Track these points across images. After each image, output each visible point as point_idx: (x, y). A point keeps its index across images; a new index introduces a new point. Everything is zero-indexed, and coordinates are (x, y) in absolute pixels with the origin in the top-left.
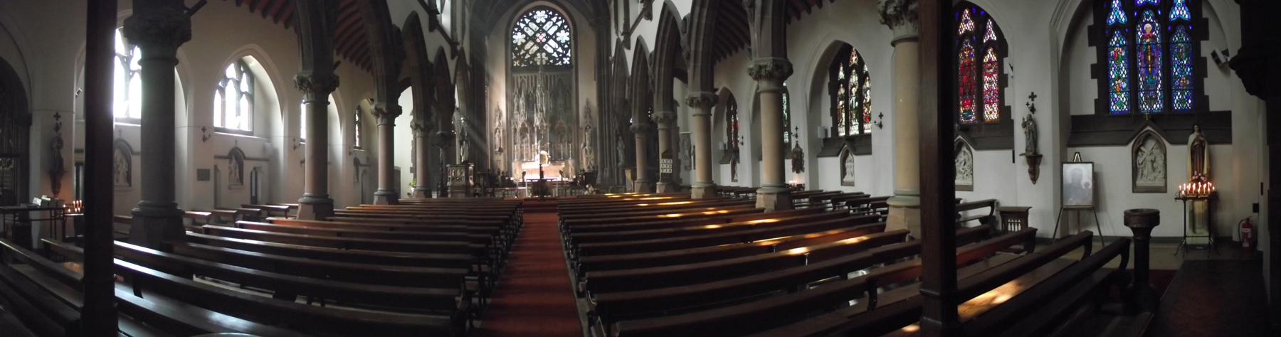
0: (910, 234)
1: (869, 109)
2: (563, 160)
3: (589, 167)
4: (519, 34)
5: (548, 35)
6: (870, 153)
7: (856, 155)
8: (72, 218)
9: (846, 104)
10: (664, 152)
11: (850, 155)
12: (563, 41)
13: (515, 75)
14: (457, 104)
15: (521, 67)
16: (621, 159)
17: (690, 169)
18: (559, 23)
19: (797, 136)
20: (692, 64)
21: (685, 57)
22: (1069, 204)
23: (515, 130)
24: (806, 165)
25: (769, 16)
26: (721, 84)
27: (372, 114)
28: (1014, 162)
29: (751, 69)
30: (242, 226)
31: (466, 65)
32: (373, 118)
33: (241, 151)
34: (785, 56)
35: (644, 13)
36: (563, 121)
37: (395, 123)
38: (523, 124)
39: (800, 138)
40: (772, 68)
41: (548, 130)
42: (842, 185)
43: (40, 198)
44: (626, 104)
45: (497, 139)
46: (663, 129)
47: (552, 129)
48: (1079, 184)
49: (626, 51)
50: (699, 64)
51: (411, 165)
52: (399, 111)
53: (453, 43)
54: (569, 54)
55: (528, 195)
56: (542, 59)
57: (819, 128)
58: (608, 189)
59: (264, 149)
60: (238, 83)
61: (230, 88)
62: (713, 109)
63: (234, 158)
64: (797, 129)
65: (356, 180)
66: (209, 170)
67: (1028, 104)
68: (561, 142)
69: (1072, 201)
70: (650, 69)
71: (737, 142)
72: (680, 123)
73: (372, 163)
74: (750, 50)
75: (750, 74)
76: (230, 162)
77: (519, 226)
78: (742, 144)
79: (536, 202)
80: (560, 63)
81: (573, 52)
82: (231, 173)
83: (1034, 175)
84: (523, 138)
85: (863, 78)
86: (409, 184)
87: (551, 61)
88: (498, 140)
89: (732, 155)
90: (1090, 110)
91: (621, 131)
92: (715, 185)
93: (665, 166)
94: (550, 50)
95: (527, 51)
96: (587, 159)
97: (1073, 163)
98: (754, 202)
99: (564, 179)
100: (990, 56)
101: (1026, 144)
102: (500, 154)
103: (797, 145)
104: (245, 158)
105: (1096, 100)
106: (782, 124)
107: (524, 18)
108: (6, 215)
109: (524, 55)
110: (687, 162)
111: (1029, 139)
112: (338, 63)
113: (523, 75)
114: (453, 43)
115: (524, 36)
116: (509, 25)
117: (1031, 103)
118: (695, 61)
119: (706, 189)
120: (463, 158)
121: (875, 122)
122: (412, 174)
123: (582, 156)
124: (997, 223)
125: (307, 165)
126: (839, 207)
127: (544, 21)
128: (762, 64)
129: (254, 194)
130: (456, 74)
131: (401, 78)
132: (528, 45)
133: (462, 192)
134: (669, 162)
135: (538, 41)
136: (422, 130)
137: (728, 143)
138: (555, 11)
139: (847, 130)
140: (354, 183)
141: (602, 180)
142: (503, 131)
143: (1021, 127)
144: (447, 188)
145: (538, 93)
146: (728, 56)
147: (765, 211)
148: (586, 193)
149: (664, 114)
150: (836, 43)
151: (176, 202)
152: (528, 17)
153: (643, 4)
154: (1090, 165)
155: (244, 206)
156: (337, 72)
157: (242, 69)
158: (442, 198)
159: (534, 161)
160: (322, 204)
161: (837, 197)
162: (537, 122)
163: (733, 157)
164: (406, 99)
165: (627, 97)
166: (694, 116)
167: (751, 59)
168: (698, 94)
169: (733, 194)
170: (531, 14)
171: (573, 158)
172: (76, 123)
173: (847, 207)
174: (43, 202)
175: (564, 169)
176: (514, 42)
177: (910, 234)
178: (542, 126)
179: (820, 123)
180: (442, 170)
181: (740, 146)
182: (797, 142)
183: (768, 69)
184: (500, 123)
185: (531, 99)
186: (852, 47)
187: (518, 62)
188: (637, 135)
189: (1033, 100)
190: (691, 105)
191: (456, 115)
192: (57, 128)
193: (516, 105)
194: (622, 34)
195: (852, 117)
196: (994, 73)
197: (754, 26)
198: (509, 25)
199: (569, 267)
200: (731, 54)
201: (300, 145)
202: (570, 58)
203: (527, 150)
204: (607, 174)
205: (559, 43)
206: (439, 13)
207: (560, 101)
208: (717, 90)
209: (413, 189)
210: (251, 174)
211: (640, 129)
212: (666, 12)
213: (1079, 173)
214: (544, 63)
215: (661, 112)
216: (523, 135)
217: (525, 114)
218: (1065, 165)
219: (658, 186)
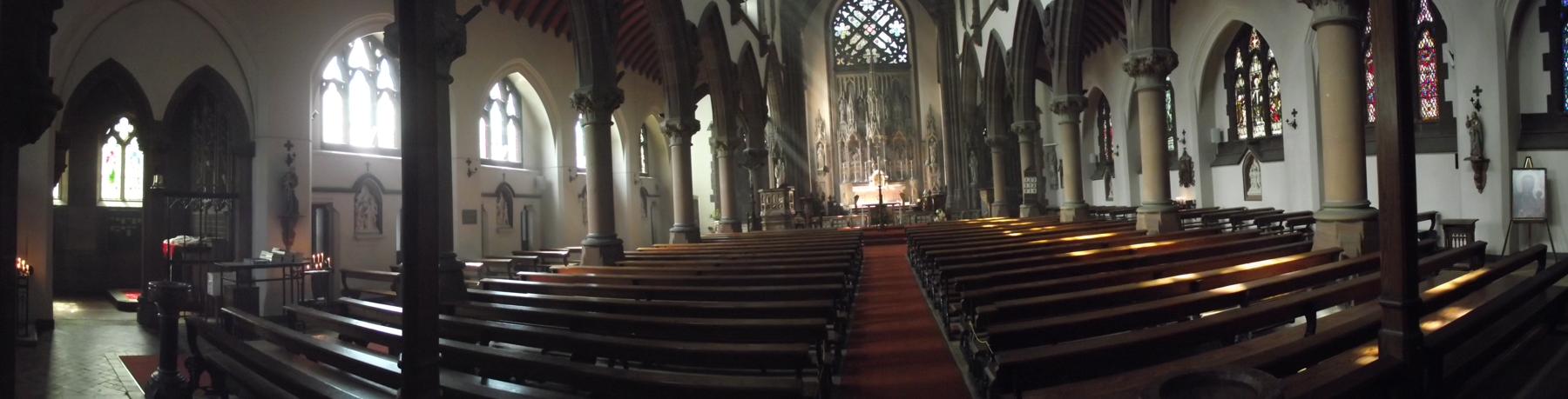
0: (1344, 253)
1: (1277, 105)
3: (934, 189)
4: (842, 24)
5: (878, 26)
6: (1282, 159)
7: (1263, 161)
8: (310, 276)
9: (1247, 99)
10: (1027, 170)
11: (1255, 162)
12: (897, 35)
13: (839, 76)
14: (769, 114)
15: (846, 65)
17: (1057, 188)
18: (892, 12)
19: (1184, 142)
20: (1056, 62)
22: (1519, 217)
23: (843, 143)
24: (1197, 177)
26: (1090, 83)
27: (663, 132)
28: (1457, 167)
29: (1126, 64)
30: (524, 278)
31: (778, 63)
32: (662, 137)
33: (511, 188)
34: (1169, 43)
37: (692, 142)
38: (852, 137)
39: (1188, 143)
41: (884, 144)
42: (1245, 199)
43: (270, 252)
45: (820, 155)
47: (888, 143)
48: (1531, 194)
49: (976, 47)
50: (1065, 62)
51: (711, 192)
52: (696, 127)
53: (761, 36)
54: (905, 50)
56: (872, 56)
57: (1212, 131)
58: (959, 214)
59: (535, 183)
60: (503, 105)
61: (495, 111)
62: (1082, 115)
63: (501, 195)
64: (1184, 133)
65: (644, 215)
66: (475, 211)
67: (1472, 100)
68: (900, 157)
69: (1523, 213)
70: (1007, 70)
71: (1110, 152)
72: (1043, 134)
73: (663, 193)
74: (1125, 41)
75: (1126, 71)
76: (498, 202)
77: (861, 263)
78: (1117, 154)
80: (895, 61)
81: (910, 47)
82: (498, 214)
83: (1480, 182)
85: (1268, 65)
86: (710, 217)
87: (884, 59)
88: (820, 157)
89: (1105, 168)
90: (1542, 108)
91: (973, 144)
92: (1088, 205)
94: (882, 46)
95: (854, 46)
96: (932, 178)
97: (1524, 169)
98: (1134, 223)
99: (907, 204)
100: (1426, 41)
101: (1472, 146)
102: (825, 174)
103: (1185, 153)
104: (515, 196)
105: (1548, 96)
106: (1165, 128)
107: (847, 6)
108: (224, 274)
109: (850, 51)
110: (1054, 179)
111: (1474, 141)
112: (622, 74)
113: (849, 76)
114: (761, 36)
115: (849, 27)
117: (1475, 98)
118: (1060, 59)
121: (1288, 121)
122: (713, 204)
123: (926, 174)
124: (1439, 238)
125: (589, 197)
126: (1241, 228)
127: (872, 9)
128: (1139, 57)
129: (524, 239)
130: (766, 80)
131: (698, 84)
132: (853, 38)
133: (780, 224)
135: (866, 33)
137: (1101, 154)
139: (1250, 132)
141: (952, 204)
142: (827, 146)
143: (1465, 127)
144: (760, 219)
145: (870, 99)
146: (1106, 43)
147: (1148, 234)
148: (936, 219)
150: (1234, 23)
154: (1543, 172)
155: (515, 253)
156: (621, 85)
157: (508, 89)
160: (609, 247)
161: (1239, 216)
162: (870, 134)
163: (1107, 170)
164: (704, 111)
165: (979, 102)
166: (1060, 124)
167: (1127, 52)
169: (1107, 215)
171: (915, 178)
172: (314, 154)
173: (1256, 227)
174: (275, 256)
176: (836, 35)
177: (1344, 253)
178: (876, 139)
179: (1213, 125)
180: (753, 197)
181: (1114, 157)
182: (1185, 149)
183: (1147, 62)
184: (822, 135)
185: (861, 105)
186: (1251, 28)
187: (842, 59)
188: (993, 150)
189: (1478, 95)
190: (1056, 112)
192: (289, 160)
193: (842, 112)
194: (972, 27)
195: (1255, 115)
196: (1432, 61)
197: (1130, 11)
199: (931, 306)
200: (1109, 42)
201: (577, 175)
203: (858, 169)
204: (958, 196)
205: (893, 36)
208: (1086, 91)
210: (522, 213)
211: (998, 143)
213: (1530, 181)
214: (875, 61)
215: (1023, 122)
216: (852, 151)
217: (854, 124)
218: (1515, 172)
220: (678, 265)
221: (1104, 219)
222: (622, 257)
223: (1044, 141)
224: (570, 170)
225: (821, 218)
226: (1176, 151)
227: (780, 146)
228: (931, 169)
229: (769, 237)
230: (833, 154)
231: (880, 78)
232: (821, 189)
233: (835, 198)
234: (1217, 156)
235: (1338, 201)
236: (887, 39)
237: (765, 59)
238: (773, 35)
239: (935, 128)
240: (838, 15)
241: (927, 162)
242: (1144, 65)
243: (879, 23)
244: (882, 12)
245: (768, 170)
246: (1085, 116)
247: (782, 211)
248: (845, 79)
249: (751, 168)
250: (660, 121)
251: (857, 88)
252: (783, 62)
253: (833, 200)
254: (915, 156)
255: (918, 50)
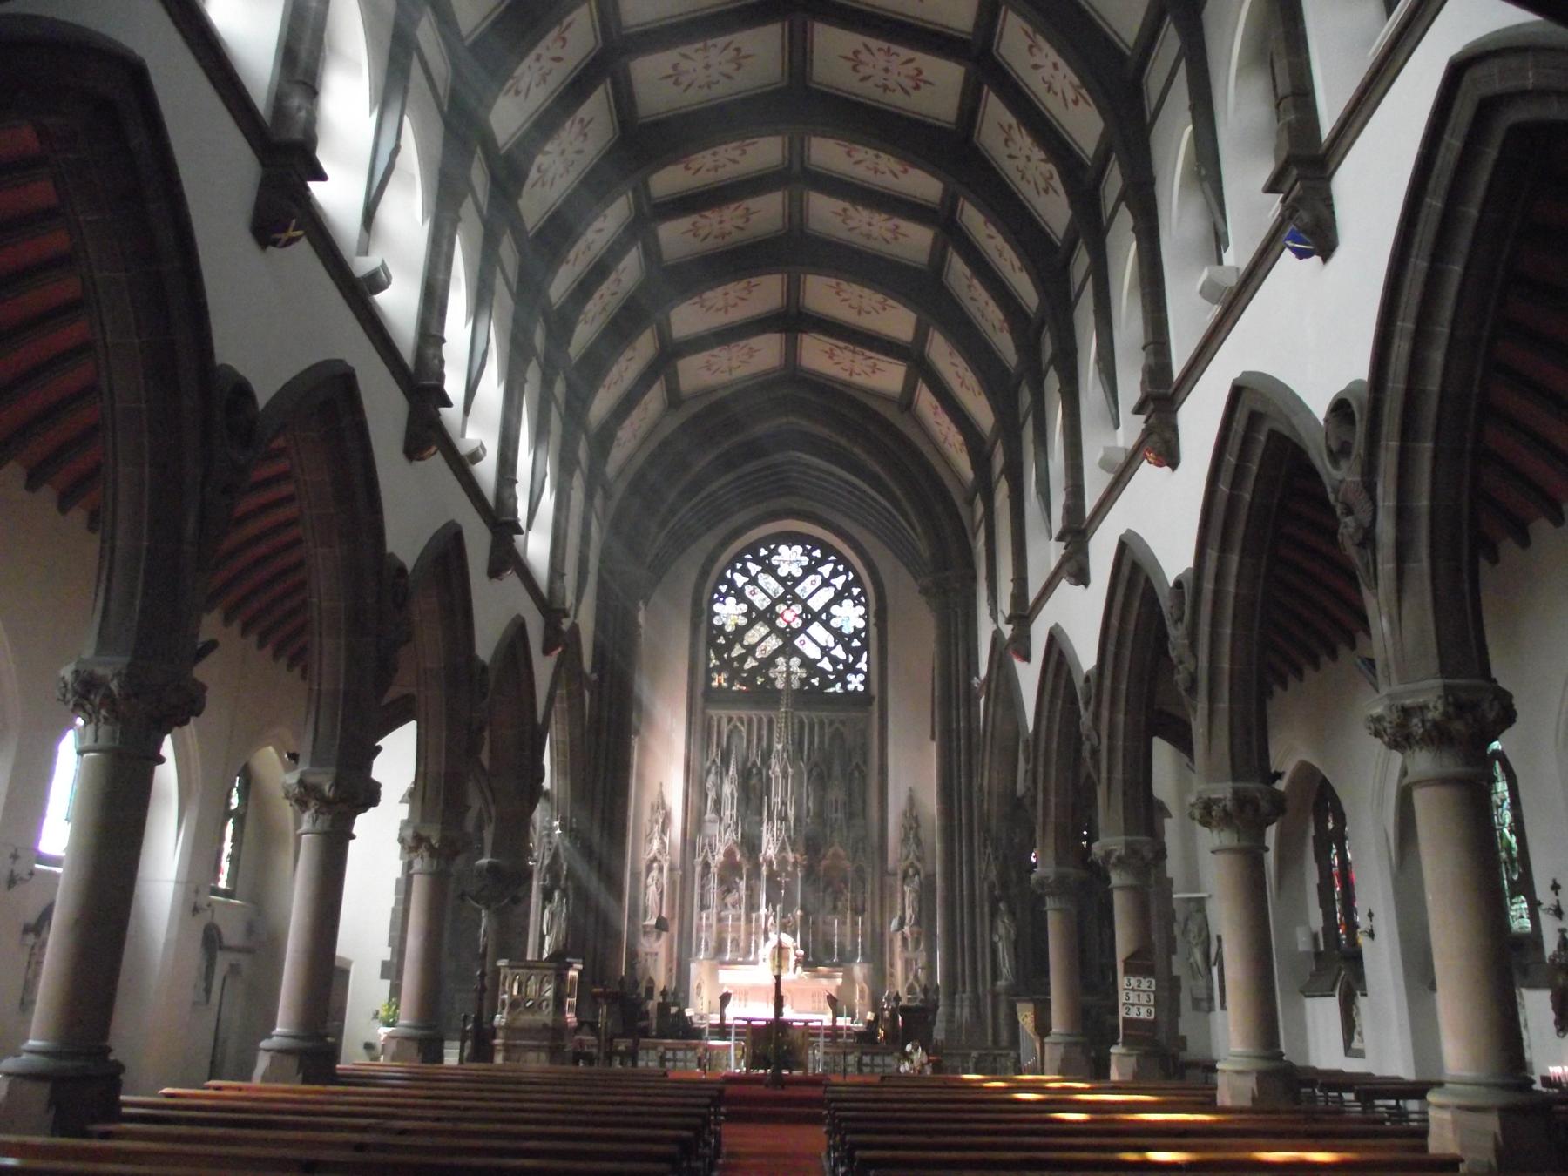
2: (838, 965)
3: (910, 990)
4: (731, 601)
5: (807, 609)
12: (848, 630)
13: (714, 713)
14: (546, 784)
16: (1006, 967)
17: (1211, 1009)
18: (839, 582)
20: (1202, 705)
21: (1181, 689)
23: (706, 865)
25: (1422, 563)
29: (1378, 719)
31: (581, 673)
32: (287, 810)
34: (1485, 671)
35: (1067, 567)
36: (842, 852)
37: (355, 831)
38: (729, 854)
40: (1445, 713)
44: (1017, 810)
45: (652, 890)
46: (1122, 888)
47: (810, 872)
49: (1019, 665)
50: (1224, 705)
51: (386, 953)
52: (369, 796)
53: (551, 609)
54: (862, 665)
55: (735, 1066)
56: (789, 673)
62: (1271, 833)
65: (202, 994)
70: (1086, 717)
71: (1352, 927)
72: (1173, 866)
74: (1371, 663)
75: (1377, 734)
78: (1371, 934)
79: (759, 1090)
80: (838, 688)
84: (729, 891)
87: (815, 681)
88: (653, 892)
91: (1005, 885)
93: (1133, 998)
94: (812, 652)
95: (751, 649)
96: (907, 963)
98: (1423, 1133)
99: (842, 1022)
102: (659, 937)
107: (744, 562)
109: (742, 659)
110: (1202, 982)
112: (211, 646)
113: (734, 713)
114: (551, 609)
115: (744, 607)
116: (704, 573)
118: (1212, 698)
119: (1263, 1077)
120: (547, 940)
122: (387, 984)
127: (798, 573)
128: (1408, 702)
130: (551, 699)
134: (1144, 986)
135: (781, 623)
136: (433, 852)
138: (828, 550)
140: (195, 1003)
141: (949, 1032)
142: (671, 870)
144: (493, 1033)
145: (776, 768)
147: (1463, 1168)
148: (905, 1067)
149: (1128, 845)
151: (108, 1044)
152: (757, 560)
153: (1063, 544)
156: (201, 672)
158: (475, 1065)
159: (755, 963)
162: (769, 850)
165: (1020, 789)
168: (1223, 791)
169: (1349, 1096)
170: (763, 552)
171: (866, 959)
175: (839, 989)
176: (716, 621)
178: (783, 862)
180: (483, 975)
181: (1363, 940)
183: (1430, 715)
184: (663, 843)
185: (754, 781)
187: (724, 676)
188: (1050, 903)
191: (540, 814)
193: (712, 795)
194: (1008, 621)
197: (1376, 595)
198: (704, 573)
200: (1317, 667)
201: (32, 873)
202: (867, 674)
203: (737, 929)
204: (964, 1013)
205: (838, 634)
206: (520, 531)
207: (836, 793)
208: (1279, 776)
209: (384, 1031)
211: (1061, 886)
212: (1126, 570)
214: (795, 685)
215: (1122, 838)
216: (727, 886)
219: (1113, 1059)
220: (265, 1142)
221: (1339, 1110)
222: (112, 1110)
223: (1176, 884)
224: (15, 857)
225: (636, 1043)
226: (1535, 938)
227: (562, 860)
228: (904, 939)
229: (504, 1081)
230: (683, 889)
231: (801, 723)
232: (646, 969)
233: (675, 994)
234: (1312, 975)
235: (1468, 1074)
236: (825, 638)
237: (552, 659)
238: (577, 610)
239: (918, 843)
240: (723, 580)
241: (895, 923)
242: (1423, 722)
243: (810, 603)
244: (818, 579)
245: (527, 915)
246: (1281, 836)
247: (546, 1016)
248: (724, 721)
249: (488, 908)
250: (288, 769)
251: (749, 741)
252: (593, 671)
253: (670, 999)
254: (868, 906)
255: (891, 666)
